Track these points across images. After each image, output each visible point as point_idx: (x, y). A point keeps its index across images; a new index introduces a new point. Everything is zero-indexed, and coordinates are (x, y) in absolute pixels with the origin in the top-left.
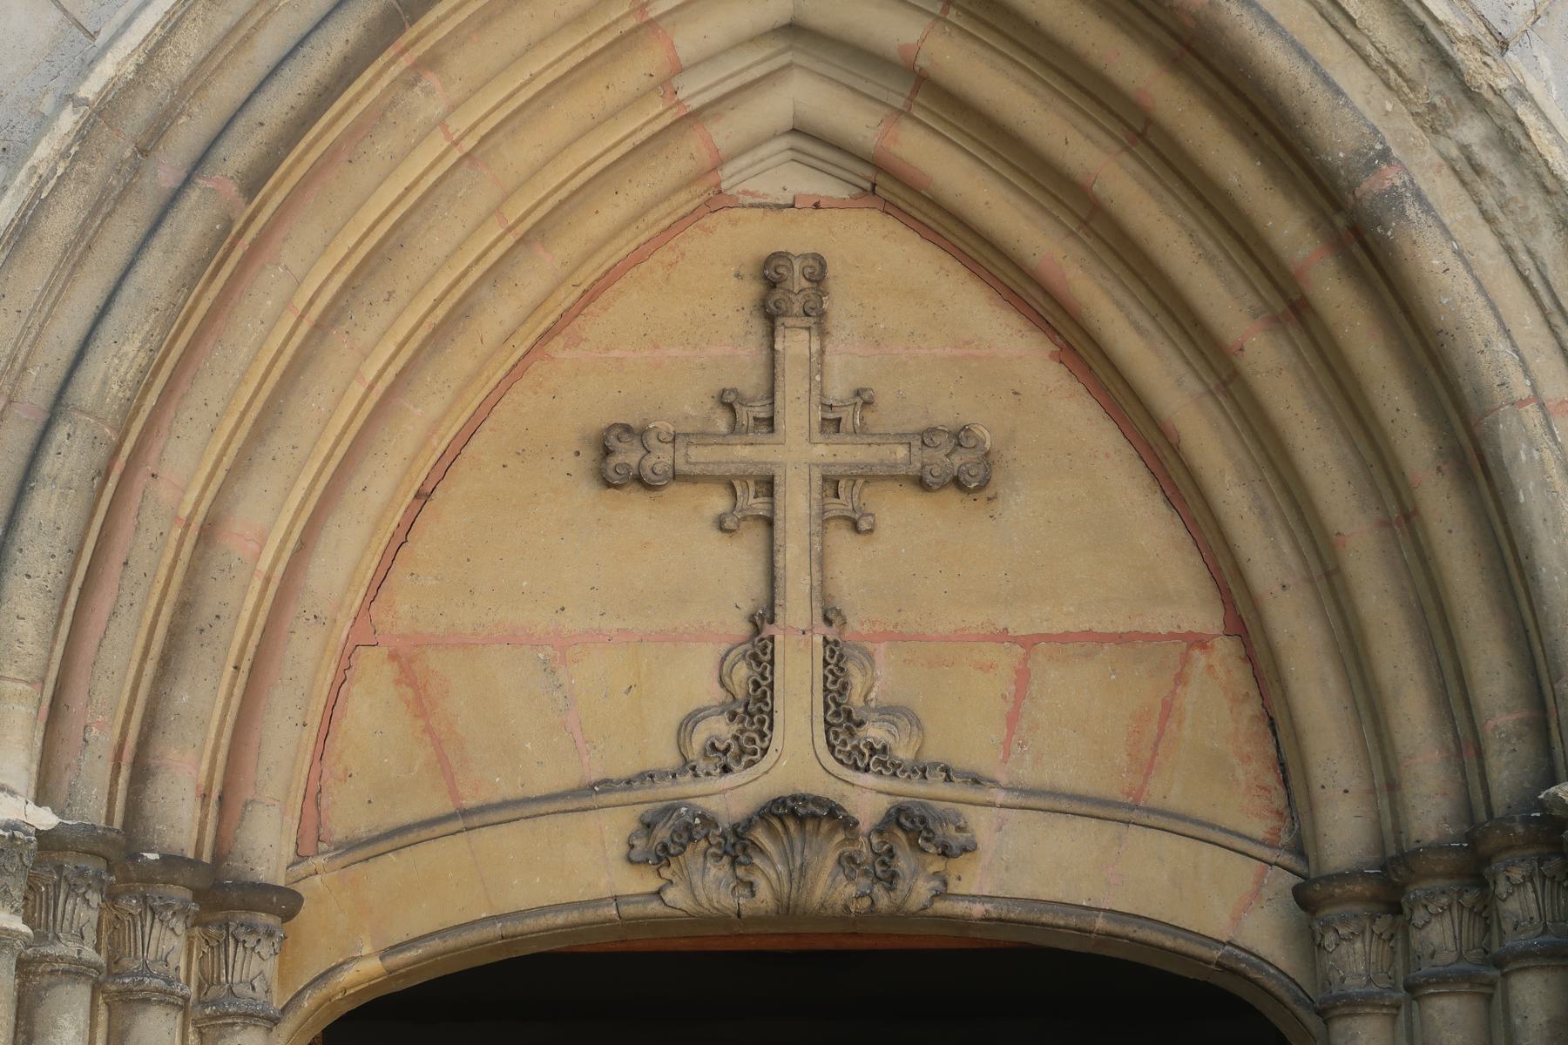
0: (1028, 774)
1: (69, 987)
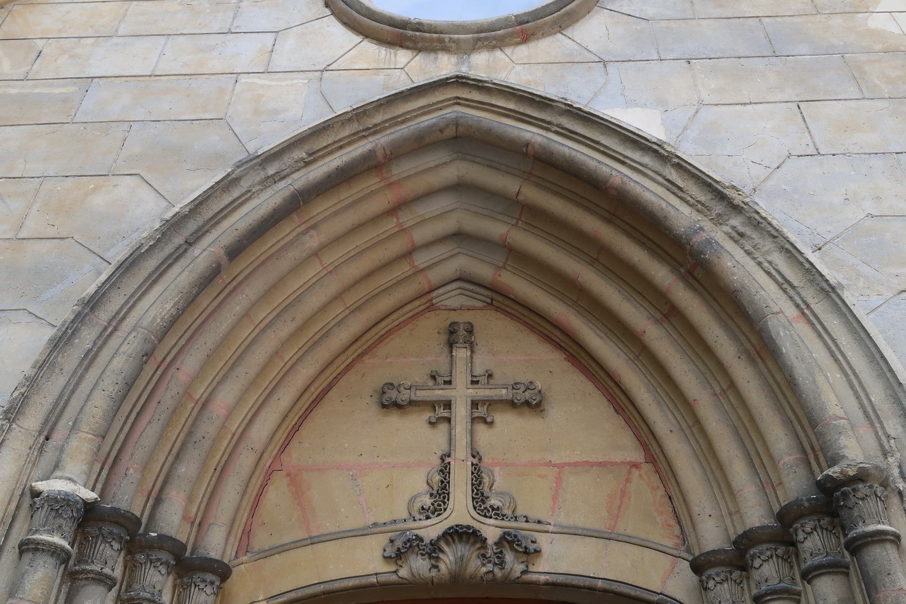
0: (562, 519)
1: (94, 587)
